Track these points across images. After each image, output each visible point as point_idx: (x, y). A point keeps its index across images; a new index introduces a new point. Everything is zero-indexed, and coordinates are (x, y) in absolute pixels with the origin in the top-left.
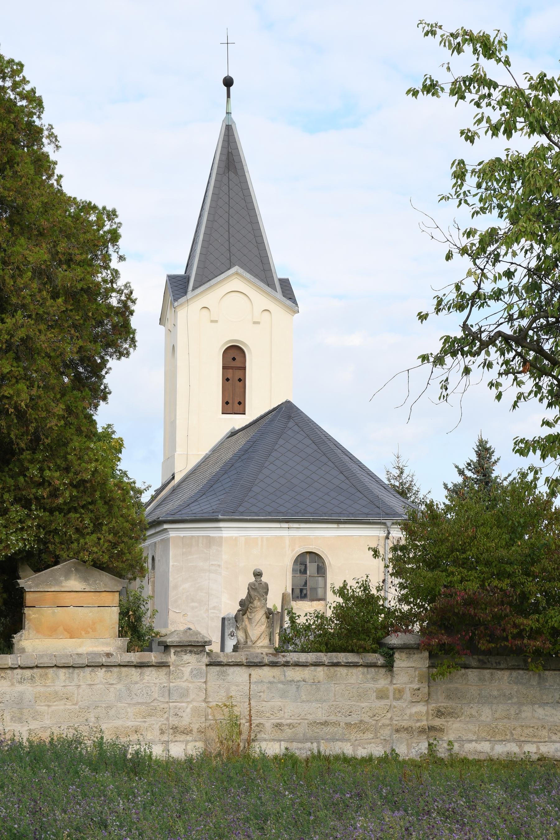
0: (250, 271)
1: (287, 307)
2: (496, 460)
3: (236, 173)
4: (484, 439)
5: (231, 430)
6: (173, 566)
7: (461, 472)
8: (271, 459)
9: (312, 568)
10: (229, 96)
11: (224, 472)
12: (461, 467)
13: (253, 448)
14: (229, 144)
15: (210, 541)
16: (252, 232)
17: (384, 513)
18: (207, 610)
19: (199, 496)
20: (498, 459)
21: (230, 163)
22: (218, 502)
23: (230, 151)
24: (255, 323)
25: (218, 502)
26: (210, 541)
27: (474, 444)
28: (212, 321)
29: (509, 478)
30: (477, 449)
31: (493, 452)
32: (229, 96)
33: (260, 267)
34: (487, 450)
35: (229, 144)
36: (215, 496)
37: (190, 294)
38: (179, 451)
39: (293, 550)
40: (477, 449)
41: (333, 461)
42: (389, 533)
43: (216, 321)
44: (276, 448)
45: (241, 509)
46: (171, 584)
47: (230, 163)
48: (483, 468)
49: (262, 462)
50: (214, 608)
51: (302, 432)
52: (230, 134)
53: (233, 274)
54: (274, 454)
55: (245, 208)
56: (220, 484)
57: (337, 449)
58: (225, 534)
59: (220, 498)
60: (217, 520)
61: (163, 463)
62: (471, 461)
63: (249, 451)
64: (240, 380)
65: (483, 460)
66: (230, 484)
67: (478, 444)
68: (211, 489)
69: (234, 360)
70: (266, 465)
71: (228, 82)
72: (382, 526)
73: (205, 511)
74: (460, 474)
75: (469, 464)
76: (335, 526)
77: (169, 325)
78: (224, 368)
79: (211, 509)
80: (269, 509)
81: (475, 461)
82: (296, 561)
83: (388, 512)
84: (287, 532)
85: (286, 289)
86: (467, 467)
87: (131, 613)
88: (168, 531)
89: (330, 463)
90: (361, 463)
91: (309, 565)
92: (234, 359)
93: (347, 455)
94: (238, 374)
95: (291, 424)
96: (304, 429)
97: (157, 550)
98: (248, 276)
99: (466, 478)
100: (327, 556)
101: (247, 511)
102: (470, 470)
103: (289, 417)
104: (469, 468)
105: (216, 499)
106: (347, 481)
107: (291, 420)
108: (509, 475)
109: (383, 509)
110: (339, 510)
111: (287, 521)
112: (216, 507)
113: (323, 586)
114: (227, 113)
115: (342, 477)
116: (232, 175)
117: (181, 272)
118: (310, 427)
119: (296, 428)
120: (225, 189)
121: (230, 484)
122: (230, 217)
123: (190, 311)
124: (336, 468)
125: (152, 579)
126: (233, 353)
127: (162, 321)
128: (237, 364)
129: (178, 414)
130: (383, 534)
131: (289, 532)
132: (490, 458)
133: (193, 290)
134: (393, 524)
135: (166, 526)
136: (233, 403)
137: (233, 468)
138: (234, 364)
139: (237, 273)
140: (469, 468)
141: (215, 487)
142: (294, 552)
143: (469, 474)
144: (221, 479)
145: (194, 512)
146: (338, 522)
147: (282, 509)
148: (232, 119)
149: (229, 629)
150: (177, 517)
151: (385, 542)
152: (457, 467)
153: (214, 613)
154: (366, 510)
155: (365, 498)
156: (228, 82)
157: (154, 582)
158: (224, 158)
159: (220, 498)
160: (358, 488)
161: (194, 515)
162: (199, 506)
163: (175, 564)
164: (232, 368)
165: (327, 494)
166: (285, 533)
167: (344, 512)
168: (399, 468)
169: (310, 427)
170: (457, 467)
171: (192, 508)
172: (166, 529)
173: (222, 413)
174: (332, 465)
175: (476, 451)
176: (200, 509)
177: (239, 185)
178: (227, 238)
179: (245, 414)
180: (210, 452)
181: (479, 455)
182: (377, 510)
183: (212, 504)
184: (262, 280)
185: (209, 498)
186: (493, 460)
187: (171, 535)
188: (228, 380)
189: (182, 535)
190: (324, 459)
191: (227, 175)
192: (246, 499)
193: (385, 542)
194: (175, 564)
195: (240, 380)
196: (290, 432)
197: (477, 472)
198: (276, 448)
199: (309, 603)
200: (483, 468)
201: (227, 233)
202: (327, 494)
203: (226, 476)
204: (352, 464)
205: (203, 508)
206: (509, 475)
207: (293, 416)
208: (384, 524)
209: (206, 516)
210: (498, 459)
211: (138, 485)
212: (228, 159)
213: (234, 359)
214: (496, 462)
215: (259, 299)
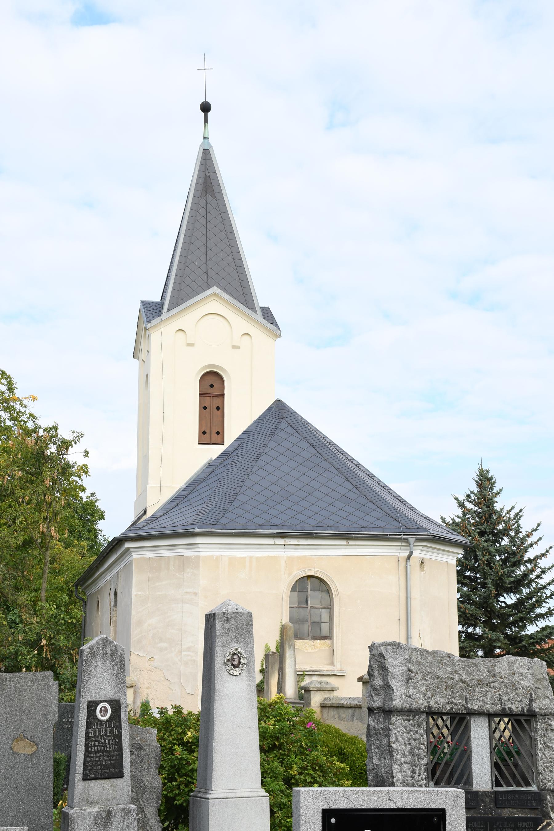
1: (270, 331)
2: (499, 491)
3: (214, 197)
4: (485, 467)
5: (209, 461)
6: (136, 595)
7: (461, 505)
8: (260, 463)
9: (314, 597)
10: (206, 121)
11: (201, 480)
12: (462, 498)
13: (237, 452)
14: (206, 168)
15: (183, 562)
16: (231, 255)
17: (404, 527)
18: (180, 652)
19: (171, 508)
20: (501, 490)
21: (207, 186)
22: (195, 513)
23: (207, 174)
24: (235, 347)
25: (195, 513)
26: (183, 562)
27: (474, 474)
28: (189, 345)
29: (513, 511)
30: (477, 479)
31: (495, 483)
32: (206, 121)
33: (240, 291)
34: (489, 479)
35: (206, 168)
36: (190, 507)
37: (164, 316)
38: (152, 483)
39: (290, 574)
40: (477, 479)
41: (336, 466)
43: (193, 345)
44: (265, 451)
45: (224, 521)
46: (134, 620)
47: (207, 186)
48: (485, 500)
49: (250, 467)
50: (189, 649)
51: (296, 434)
52: (208, 158)
53: (210, 295)
54: (264, 458)
55: (224, 231)
56: (197, 493)
57: (339, 454)
59: (196, 508)
60: (193, 535)
61: (135, 502)
62: (472, 492)
63: (232, 455)
65: (485, 490)
66: (210, 492)
67: (479, 474)
68: (186, 499)
69: (212, 387)
70: (254, 470)
71: (206, 108)
73: (177, 524)
74: (460, 506)
75: (469, 496)
76: (344, 542)
77: (143, 356)
78: (201, 395)
79: (185, 521)
80: (261, 521)
81: (476, 492)
82: (294, 589)
83: (409, 525)
84: (283, 550)
85: (267, 314)
86: (467, 499)
87: (44, 642)
88: (131, 552)
89: (332, 469)
90: (369, 472)
91: (311, 591)
92: (212, 386)
93: (352, 462)
94: (217, 402)
95: (283, 425)
96: (299, 431)
97: (119, 580)
98: (227, 297)
99: (466, 511)
100: (333, 582)
101: (230, 523)
102: (470, 502)
103: (281, 418)
104: (470, 500)
105: (193, 510)
106: (355, 490)
107: (283, 421)
108: (513, 508)
109: (402, 522)
110: (348, 523)
111: (283, 536)
112: (191, 518)
113: (328, 620)
114: (204, 138)
116: (209, 198)
117: (158, 299)
118: (306, 429)
119: (289, 430)
120: (203, 211)
121: (210, 492)
122: (208, 240)
123: (163, 335)
124: (340, 475)
125: (114, 619)
127: (135, 355)
129: (150, 443)
130: (406, 553)
131: (286, 550)
132: (491, 489)
133: (169, 310)
134: (418, 540)
135: (127, 545)
136: (211, 433)
137: (213, 475)
138: (211, 391)
139: (215, 294)
140: (470, 500)
141: (189, 497)
142: (291, 577)
143: (469, 506)
144: (198, 488)
145: (163, 526)
147: (276, 521)
149: (226, 645)
150: (142, 533)
151: (407, 564)
152: (456, 499)
153: (188, 655)
154: (382, 524)
155: (378, 510)
156: (206, 108)
157: (115, 622)
158: (201, 181)
159: (196, 508)
160: (370, 498)
161: (164, 529)
162: (170, 519)
163: (139, 593)
164: (209, 395)
167: (354, 525)
169: (306, 429)
170: (456, 499)
171: (161, 522)
172: (128, 549)
173: (199, 444)
174: (337, 472)
175: (476, 482)
176: (172, 522)
177: (217, 208)
179: (223, 444)
180: (185, 484)
181: (480, 486)
182: (395, 523)
183: (186, 516)
185: (182, 510)
187: (134, 557)
188: (205, 408)
189: (148, 556)
190: (325, 464)
191: (205, 198)
192: (230, 509)
193: (407, 564)
194: (139, 593)
195: (218, 408)
196: (282, 434)
197: (478, 504)
198: (265, 451)
200: (485, 500)
201: (205, 255)
203: (204, 484)
204: (358, 471)
205: (174, 521)
206: (513, 508)
207: (284, 416)
208: (406, 541)
209: (179, 530)
210: (501, 490)
211: (64, 434)
212: (205, 182)
213: (212, 386)
214: (498, 493)
215: (239, 322)
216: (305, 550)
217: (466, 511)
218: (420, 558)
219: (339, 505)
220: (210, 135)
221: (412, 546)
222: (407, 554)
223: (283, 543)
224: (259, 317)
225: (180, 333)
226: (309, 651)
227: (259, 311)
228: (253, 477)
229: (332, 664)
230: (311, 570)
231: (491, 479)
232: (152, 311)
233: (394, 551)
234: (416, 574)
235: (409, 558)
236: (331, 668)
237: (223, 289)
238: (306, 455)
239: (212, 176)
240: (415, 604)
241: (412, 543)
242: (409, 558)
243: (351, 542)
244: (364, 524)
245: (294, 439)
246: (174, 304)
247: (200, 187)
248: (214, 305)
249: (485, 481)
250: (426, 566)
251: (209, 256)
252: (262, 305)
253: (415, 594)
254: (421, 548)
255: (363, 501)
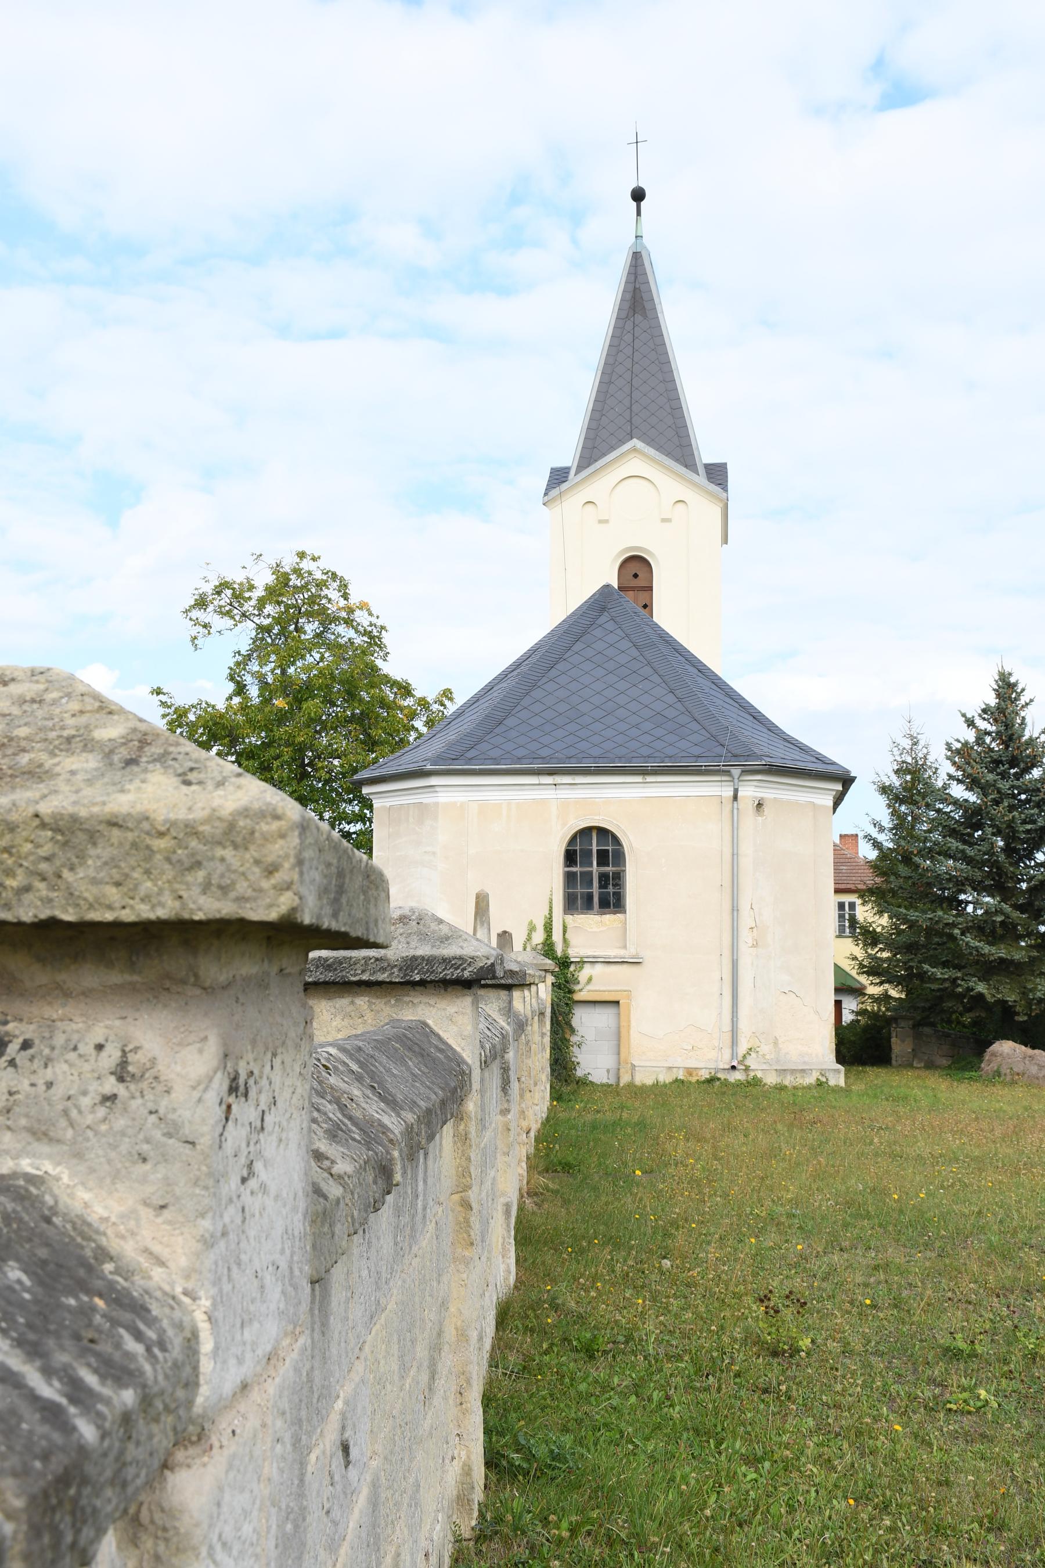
0: (659, 448)
1: (711, 494)
3: (645, 316)
4: (1007, 669)
7: (970, 723)
10: (639, 213)
14: (636, 277)
20: (1031, 701)
21: (637, 303)
24: (664, 520)
28: (600, 522)
32: (639, 213)
33: (674, 442)
34: (1012, 686)
35: (636, 277)
41: (661, 673)
42: (736, 791)
43: (606, 521)
44: (565, 657)
47: (637, 303)
53: (629, 451)
58: (444, 797)
64: (645, 606)
67: (997, 678)
71: (638, 195)
72: (724, 778)
76: (639, 779)
80: (521, 752)
83: (738, 752)
84: (553, 792)
86: (980, 715)
92: (636, 576)
93: (694, 666)
94: (642, 597)
102: (984, 719)
111: (551, 772)
115: (671, 699)
119: (611, 626)
120: (628, 338)
126: (634, 567)
128: (640, 582)
131: (558, 792)
139: (634, 450)
143: (983, 725)
146: (644, 772)
148: (642, 244)
152: (964, 715)
156: (638, 195)
158: (628, 296)
160: (696, 715)
164: (632, 589)
165: (636, 726)
166: (549, 794)
168: (912, 737)
170: (964, 715)
174: (658, 680)
178: (628, 404)
181: (999, 696)
182: (719, 750)
184: (677, 460)
186: (1022, 702)
189: (388, 805)
190: (647, 671)
195: (645, 606)
199: (597, 918)
202: (636, 726)
208: (728, 773)
210: (1031, 701)
212: (634, 297)
213: (636, 576)
216: (505, 793)
217: (981, 735)
218: (756, 798)
219: (647, 726)
220: (645, 232)
221: (736, 781)
222: (732, 793)
223: (551, 782)
224: (702, 479)
225: (590, 506)
226: (595, 929)
227: (701, 470)
228: (537, 694)
229: (625, 947)
230: (593, 819)
231: (1015, 685)
232: (558, 477)
233: (710, 790)
234: (749, 820)
235: (735, 798)
236: (622, 952)
237: (650, 442)
238: (623, 659)
239: (643, 288)
240: (746, 862)
241: (736, 777)
242: (735, 798)
243: (650, 779)
244: (670, 751)
245: (611, 638)
246: (580, 468)
247: (627, 305)
248: (635, 465)
249: (1007, 689)
250: (766, 809)
251: (638, 400)
252: (707, 460)
253: (746, 848)
254: (755, 783)
255: (684, 719)
